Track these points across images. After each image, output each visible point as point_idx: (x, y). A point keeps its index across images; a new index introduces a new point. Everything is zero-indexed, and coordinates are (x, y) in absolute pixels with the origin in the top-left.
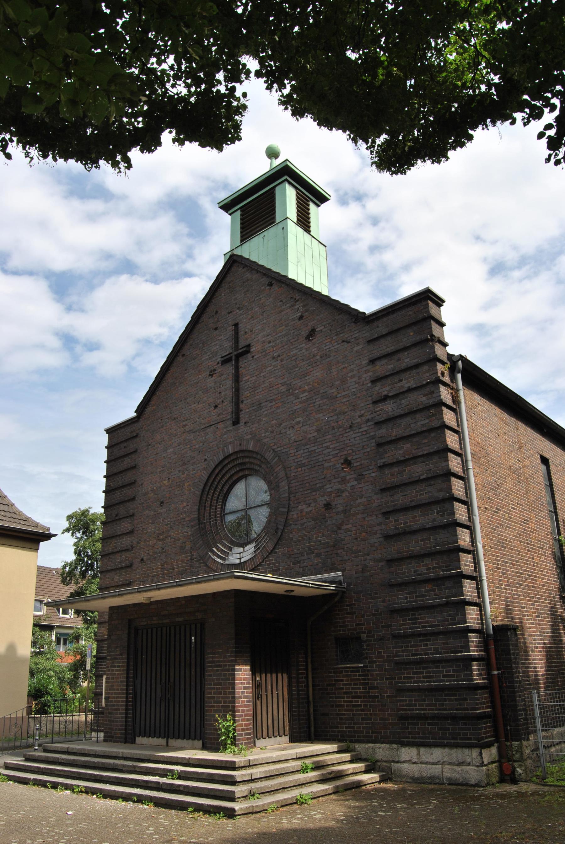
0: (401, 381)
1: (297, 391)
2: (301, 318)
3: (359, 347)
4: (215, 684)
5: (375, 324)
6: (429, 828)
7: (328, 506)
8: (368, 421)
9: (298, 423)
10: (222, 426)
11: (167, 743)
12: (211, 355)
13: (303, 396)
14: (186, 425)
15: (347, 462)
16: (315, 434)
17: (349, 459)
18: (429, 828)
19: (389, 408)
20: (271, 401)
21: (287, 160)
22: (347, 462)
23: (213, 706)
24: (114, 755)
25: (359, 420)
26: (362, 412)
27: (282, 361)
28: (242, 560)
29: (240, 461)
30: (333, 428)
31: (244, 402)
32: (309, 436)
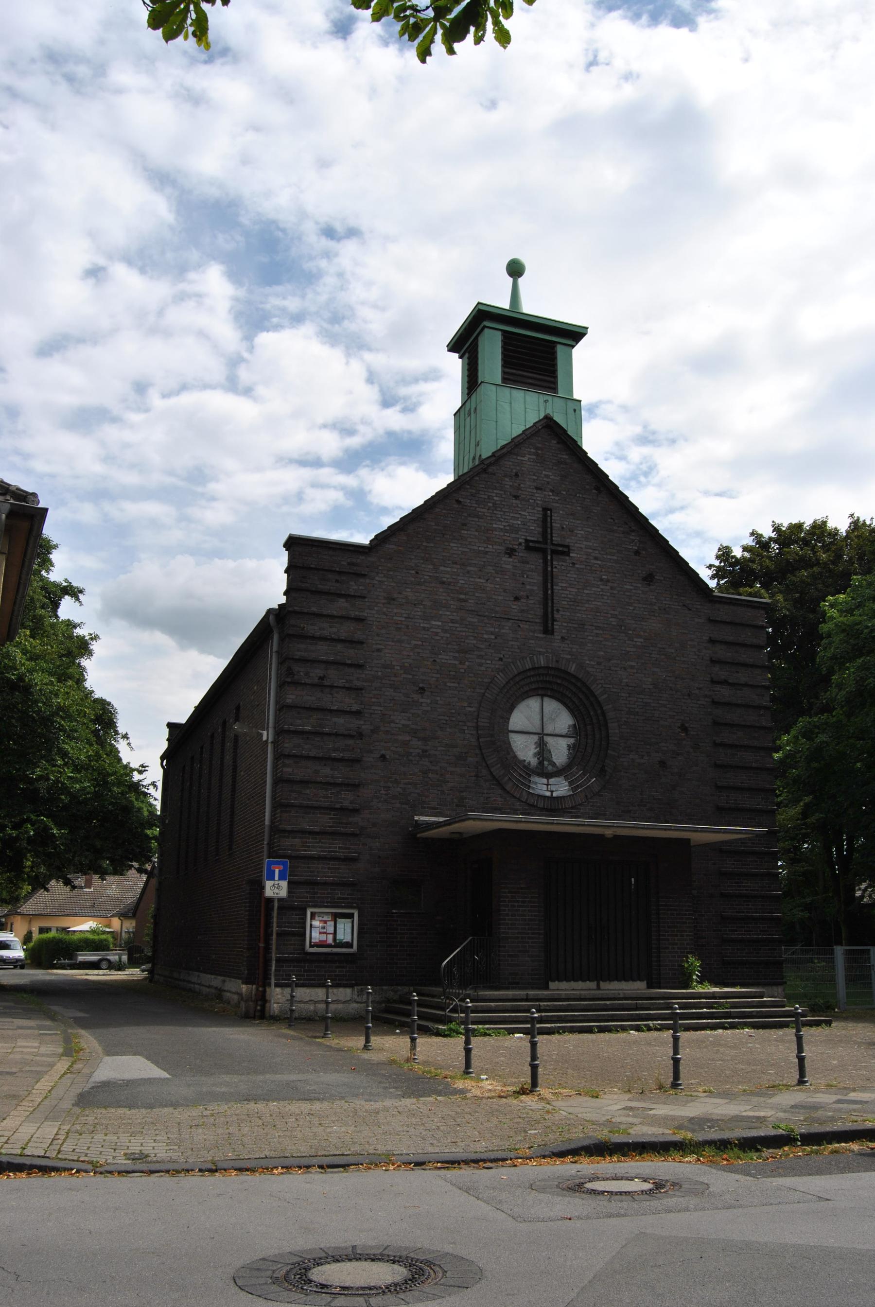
0: (737, 672)
1: (630, 632)
2: (637, 553)
3: (700, 620)
4: (669, 927)
5: (717, 606)
6: (643, 1047)
7: (663, 764)
8: (706, 696)
9: (632, 667)
10: (527, 627)
11: (598, 985)
12: (508, 528)
13: (639, 641)
14: (465, 601)
15: (684, 729)
16: (651, 687)
17: (687, 725)
18: (643, 1047)
19: (725, 693)
20: (597, 628)
21: (479, 303)
22: (684, 729)
23: (668, 948)
24: (556, 997)
25: (697, 692)
26: (701, 686)
27: (612, 588)
28: (555, 795)
29: (548, 679)
30: (671, 689)
31: (561, 613)
32: (644, 686)
